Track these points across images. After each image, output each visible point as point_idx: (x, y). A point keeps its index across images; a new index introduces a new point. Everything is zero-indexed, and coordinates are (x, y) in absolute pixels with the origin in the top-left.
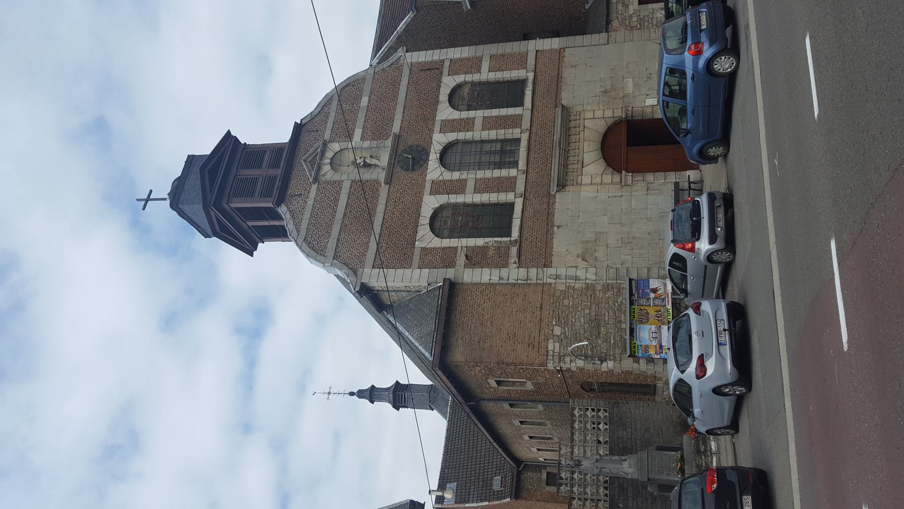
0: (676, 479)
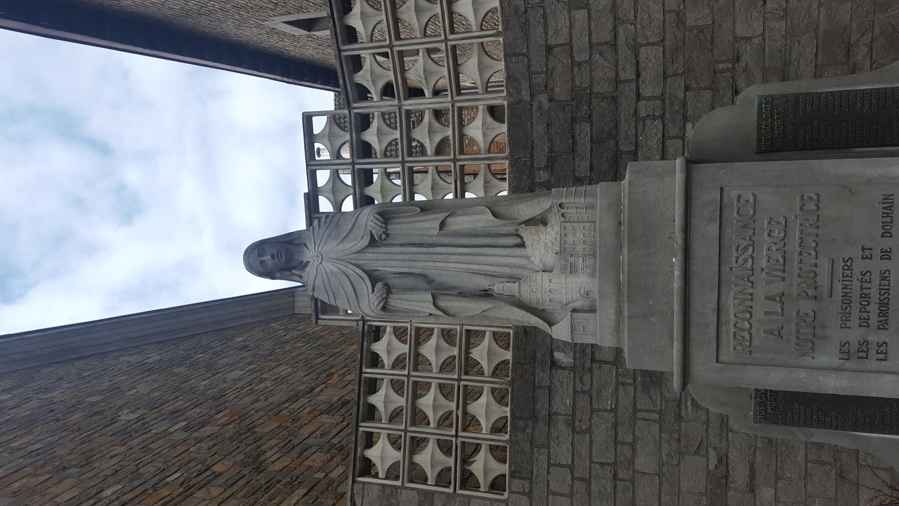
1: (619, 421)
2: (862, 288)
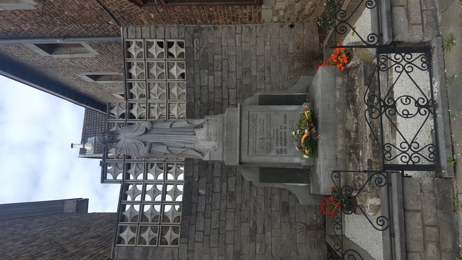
0: (297, 160)
1: (221, 213)
2: (280, 136)
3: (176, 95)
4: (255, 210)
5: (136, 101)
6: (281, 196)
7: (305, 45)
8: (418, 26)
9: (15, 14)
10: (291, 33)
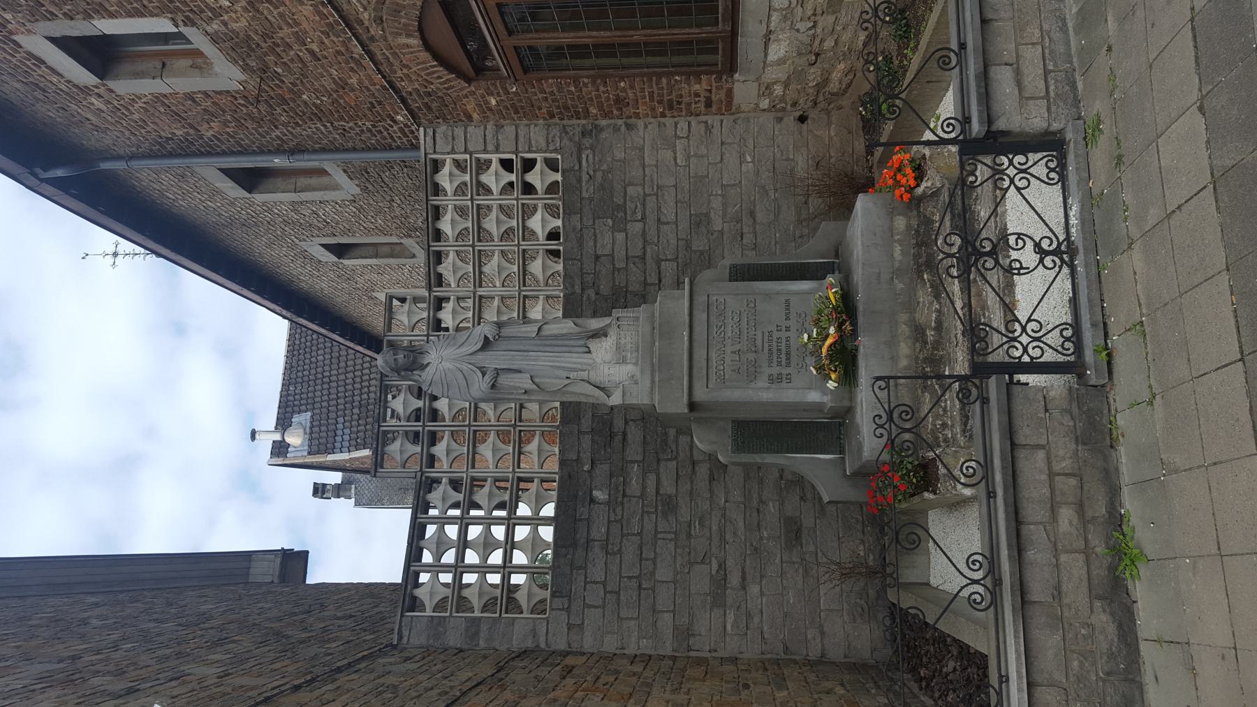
0: (814, 396)
3: (541, 278)
4: (721, 535)
5: (451, 291)
6: (782, 504)
7: (833, 160)
8: (1038, 102)
9: (193, 100)
10: (800, 134)
